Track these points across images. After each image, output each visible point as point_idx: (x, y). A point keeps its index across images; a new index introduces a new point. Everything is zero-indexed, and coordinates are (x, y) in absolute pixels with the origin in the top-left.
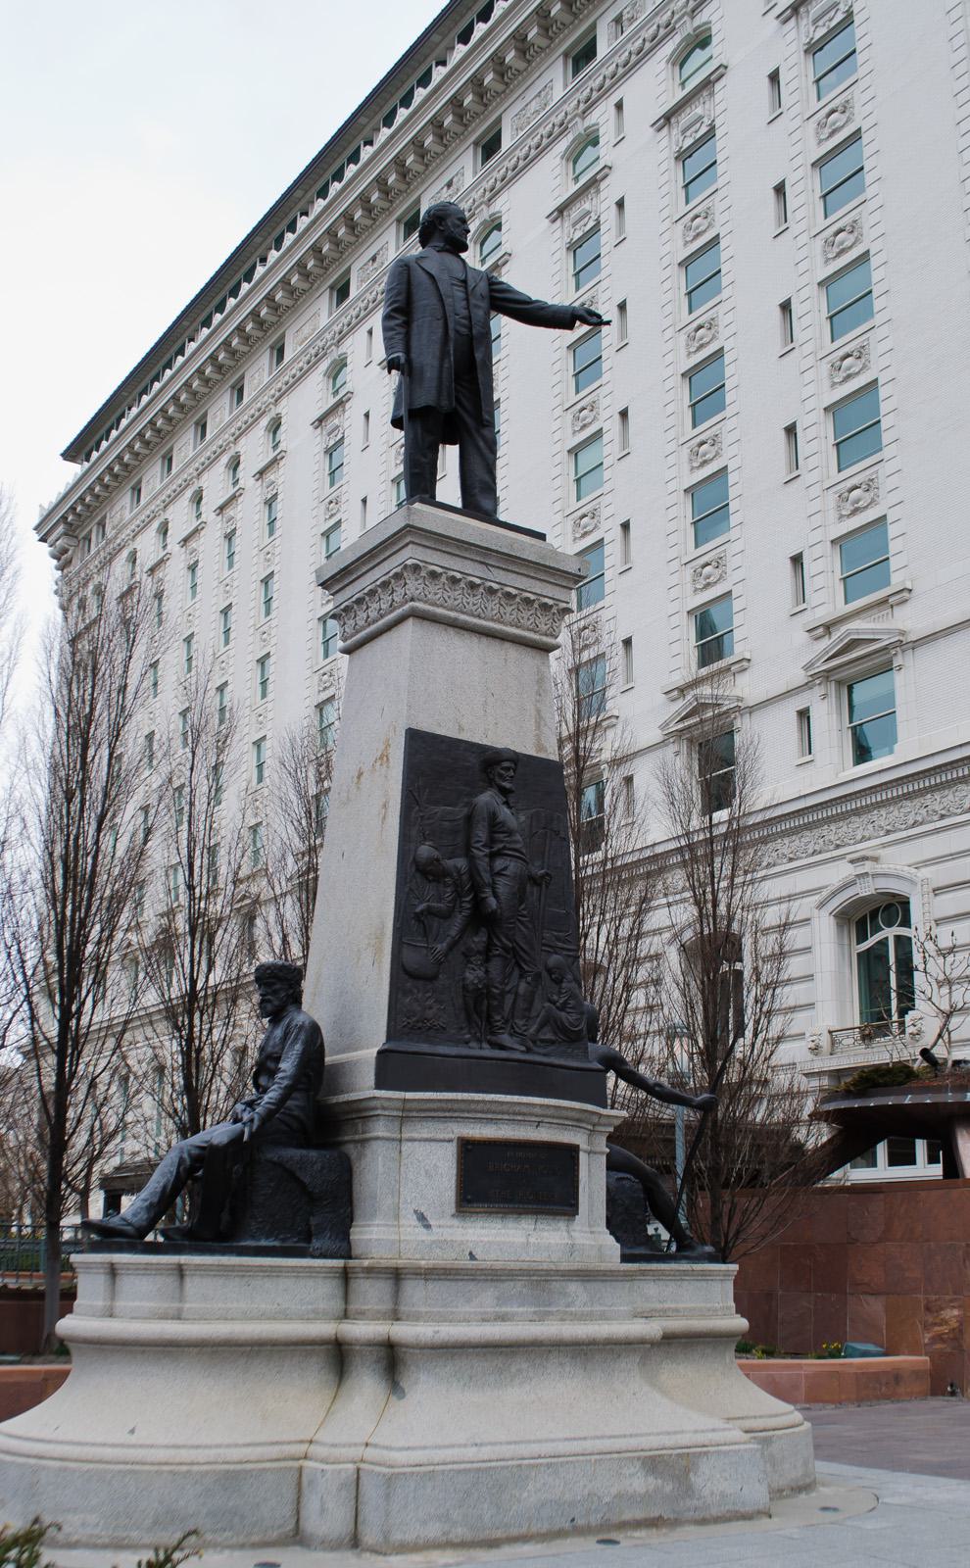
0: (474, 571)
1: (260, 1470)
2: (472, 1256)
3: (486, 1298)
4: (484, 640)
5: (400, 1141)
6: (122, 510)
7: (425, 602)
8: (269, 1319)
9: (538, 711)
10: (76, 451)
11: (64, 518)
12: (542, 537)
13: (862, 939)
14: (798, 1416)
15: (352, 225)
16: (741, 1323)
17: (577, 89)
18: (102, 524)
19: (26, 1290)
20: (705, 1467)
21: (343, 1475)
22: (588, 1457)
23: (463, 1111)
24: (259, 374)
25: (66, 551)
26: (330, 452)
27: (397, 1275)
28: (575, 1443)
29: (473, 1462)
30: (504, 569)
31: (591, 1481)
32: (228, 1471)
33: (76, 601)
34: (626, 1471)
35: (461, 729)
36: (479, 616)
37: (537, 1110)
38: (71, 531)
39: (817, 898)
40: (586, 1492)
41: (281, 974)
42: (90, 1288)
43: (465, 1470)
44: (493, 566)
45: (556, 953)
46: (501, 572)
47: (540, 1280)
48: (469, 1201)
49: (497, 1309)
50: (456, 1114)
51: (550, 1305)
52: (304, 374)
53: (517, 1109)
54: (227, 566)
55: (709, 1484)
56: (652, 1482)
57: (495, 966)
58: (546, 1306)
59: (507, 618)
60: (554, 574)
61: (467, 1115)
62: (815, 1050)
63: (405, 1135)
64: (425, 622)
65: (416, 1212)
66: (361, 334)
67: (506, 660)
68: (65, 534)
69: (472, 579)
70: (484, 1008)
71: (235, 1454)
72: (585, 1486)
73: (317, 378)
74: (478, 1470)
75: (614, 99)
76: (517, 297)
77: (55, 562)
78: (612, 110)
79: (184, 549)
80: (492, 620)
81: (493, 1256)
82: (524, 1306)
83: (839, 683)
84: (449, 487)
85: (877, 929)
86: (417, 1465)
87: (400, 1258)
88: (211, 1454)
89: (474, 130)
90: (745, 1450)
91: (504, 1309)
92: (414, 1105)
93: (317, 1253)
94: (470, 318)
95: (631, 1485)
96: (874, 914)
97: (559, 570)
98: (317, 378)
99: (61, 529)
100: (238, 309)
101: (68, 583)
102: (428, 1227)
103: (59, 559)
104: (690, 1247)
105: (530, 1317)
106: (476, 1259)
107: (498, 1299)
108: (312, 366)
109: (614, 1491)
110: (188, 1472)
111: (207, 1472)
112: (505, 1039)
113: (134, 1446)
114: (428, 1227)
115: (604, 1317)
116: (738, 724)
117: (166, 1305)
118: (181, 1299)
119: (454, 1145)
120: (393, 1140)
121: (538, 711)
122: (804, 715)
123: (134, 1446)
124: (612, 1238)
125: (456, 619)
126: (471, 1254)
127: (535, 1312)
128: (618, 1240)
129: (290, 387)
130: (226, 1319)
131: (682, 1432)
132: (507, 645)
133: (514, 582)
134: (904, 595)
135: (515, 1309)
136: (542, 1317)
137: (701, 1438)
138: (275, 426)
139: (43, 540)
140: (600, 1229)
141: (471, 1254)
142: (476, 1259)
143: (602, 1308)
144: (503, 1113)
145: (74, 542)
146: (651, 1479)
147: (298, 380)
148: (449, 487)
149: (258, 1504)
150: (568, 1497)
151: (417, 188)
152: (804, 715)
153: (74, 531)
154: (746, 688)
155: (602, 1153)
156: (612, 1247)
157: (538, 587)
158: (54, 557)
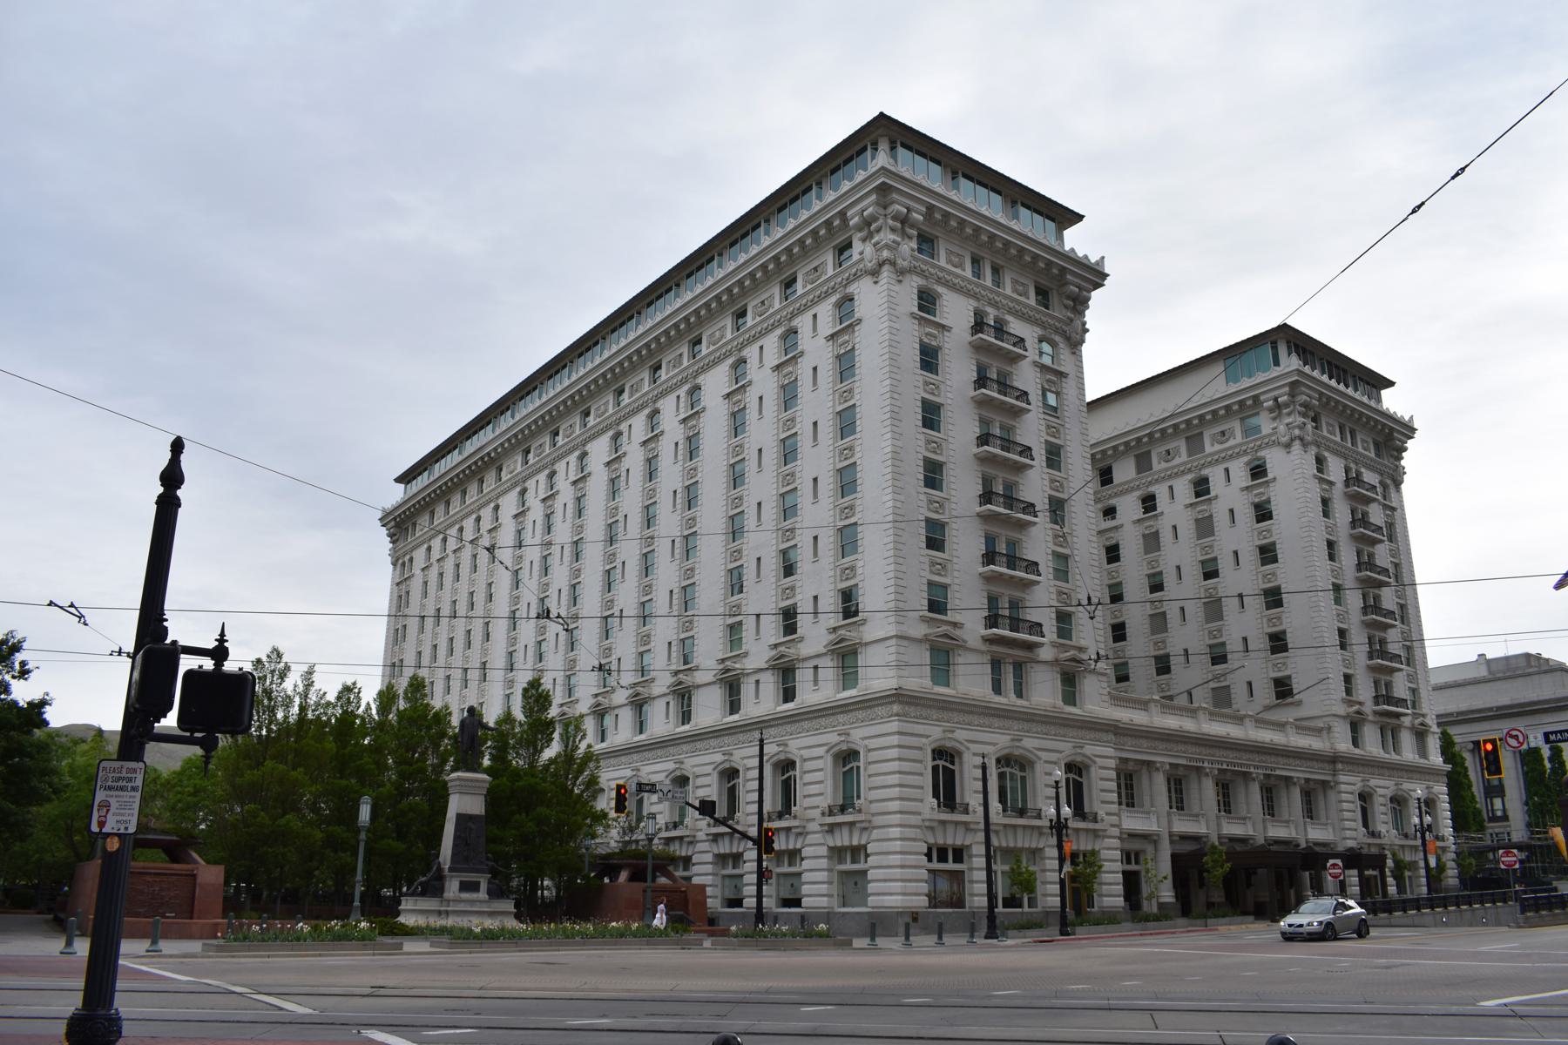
3: (462, 904)
13: (783, 775)
15: (597, 385)
17: (653, 390)
18: (414, 525)
19: (1384, 912)
26: (734, 415)
27: (449, 901)
38: (397, 526)
39: (825, 748)
42: (403, 903)
47: (472, 902)
54: (688, 458)
62: (823, 814)
66: (672, 398)
75: (759, 344)
78: (675, 399)
79: (682, 426)
83: (838, 654)
85: (788, 772)
96: (849, 755)
99: (393, 523)
101: (395, 552)
116: (859, 650)
122: (668, 703)
134: (746, 654)
152: (668, 703)
154: (805, 649)
158: (388, 536)
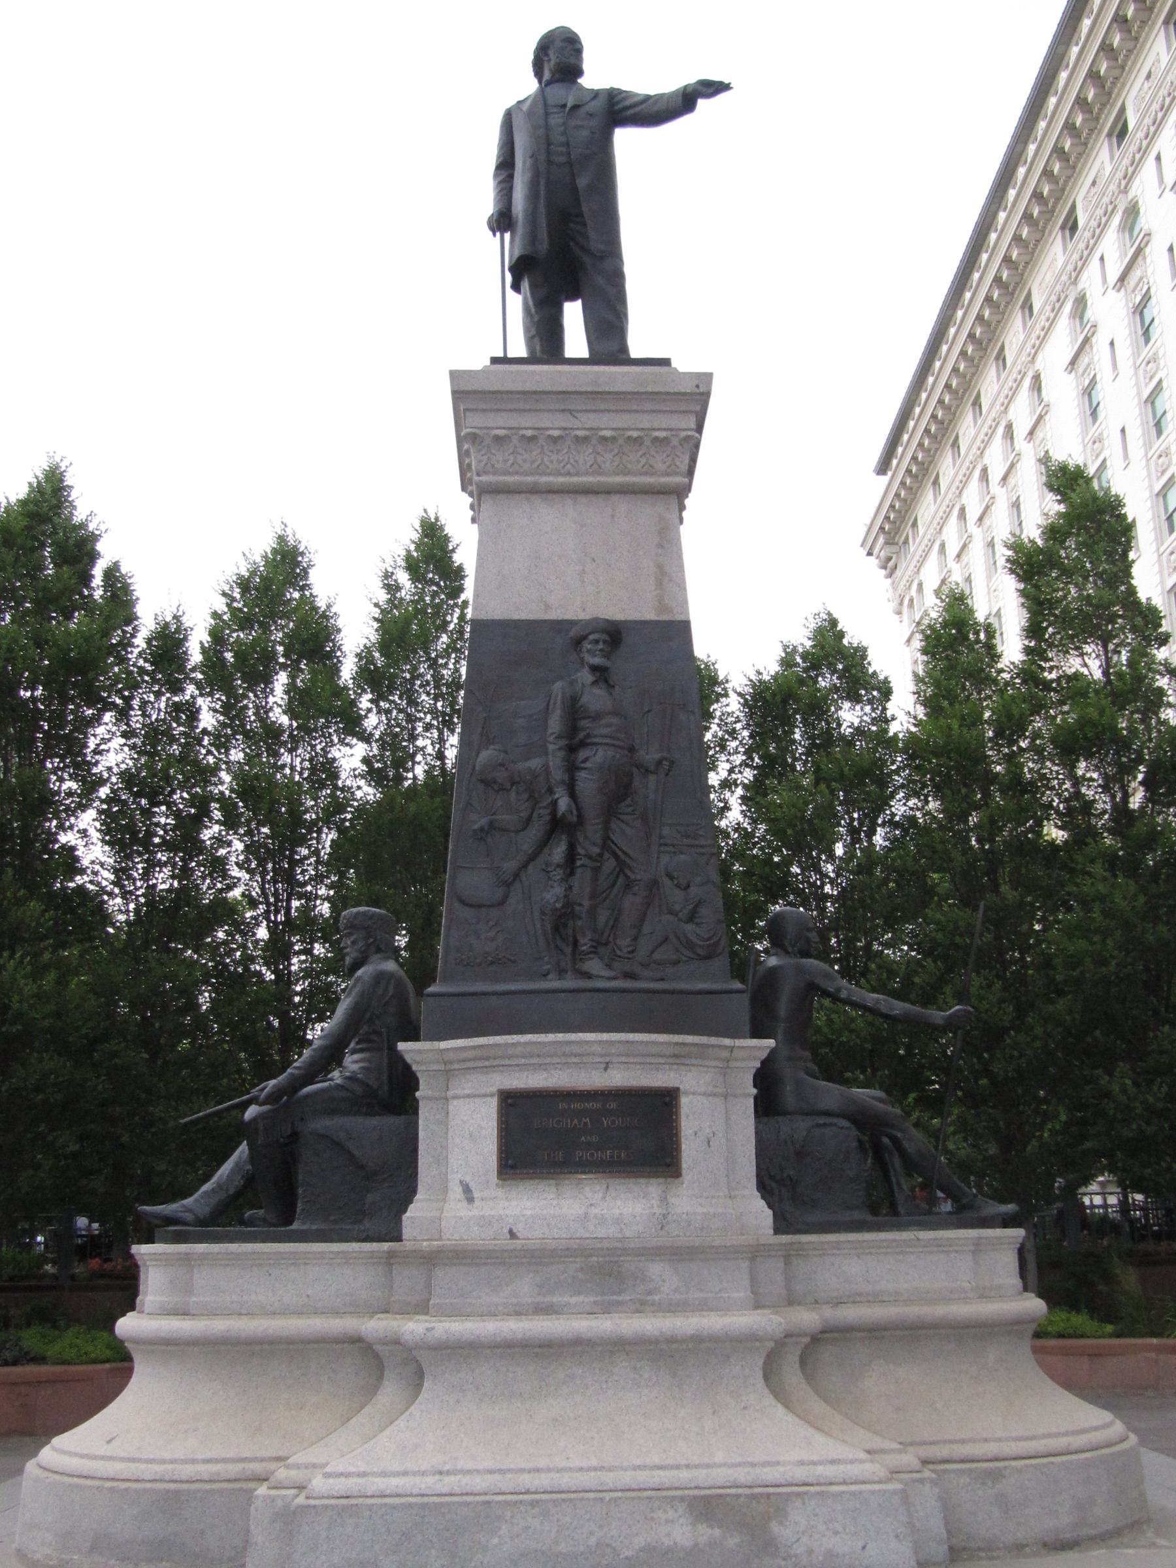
0: (553, 423)
1: (206, 1491)
2: (512, 1235)
4: (582, 499)
5: (446, 1099)
6: (927, 508)
7: (495, 473)
8: (294, 1313)
9: (660, 567)
10: (883, 467)
11: (882, 528)
12: (665, 362)
14: (1119, 1427)
16: (1035, 1305)
20: (798, 1516)
21: (279, 1502)
22: (601, 1495)
23: (503, 1058)
24: (1015, 336)
25: (889, 559)
28: (1054, 1430)
29: (423, 1495)
30: (595, 411)
31: (601, 1527)
32: (168, 1491)
33: (906, 602)
34: (660, 1515)
35: (547, 607)
36: (569, 474)
37: (597, 1049)
40: (593, 1541)
41: (356, 922)
43: (410, 1506)
44: (581, 411)
45: (682, 853)
46: (592, 416)
48: (512, 1167)
49: (540, 1299)
50: (496, 1062)
51: (620, 1293)
52: (1052, 322)
53: (567, 1049)
55: (805, 1539)
56: (706, 1533)
57: (581, 881)
58: (614, 1294)
59: (661, 466)
60: (664, 400)
61: (507, 1062)
63: (450, 1094)
64: (500, 496)
65: (461, 1182)
67: (613, 516)
68: (887, 543)
69: (524, 432)
70: (570, 932)
71: (187, 1471)
72: (592, 1533)
73: (1064, 322)
74: (424, 1506)
76: (639, 98)
77: (883, 572)
80: (587, 474)
81: (537, 1234)
82: (579, 1294)
84: (576, 342)
86: (342, 1497)
87: (440, 1239)
88: (158, 1469)
89: (1160, 10)
90: (873, 1492)
91: (548, 1299)
92: (451, 1056)
93: (363, 1236)
94: (567, 144)
95: (668, 1535)
97: (668, 393)
98: (1064, 322)
99: (881, 540)
100: (983, 282)
102: (470, 1200)
103: (885, 568)
104: (970, 1207)
105: (588, 1309)
106: (517, 1238)
107: (540, 1286)
108: (1057, 311)
109: (639, 1542)
110: (126, 1490)
111: (145, 1490)
112: (594, 965)
113: (111, 1458)
114: (470, 1200)
115: (704, 1306)
117: (176, 1299)
118: (188, 1290)
119: (494, 1102)
120: (437, 1099)
121: (660, 567)
123: (111, 1458)
124: (763, 1203)
125: (536, 484)
126: (511, 1232)
127: (595, 1302)
128: (770, 1206)
129: (1043, 340)
130: (240, 1314)
131: (778, 1463)
132: (615, 498)
133: (607, 423)
135: (566, 1299)
136: (607, 1309)
137: (800, 1474)
138: (1037, 384)
139: (870, 554)
140: (746, 1192)
141: (511, 1232)
142: (517, 1238)
143: (702, 1295)
144: (551, 1056)
145: (895, 549)
146: (702, 1528)
147: (1047, 331)
148: (576, 342)
149: (202, 1532)
150: (563, 1547)
151: (1119, 94)
153: (894, 538)
155: (749, 1095)
156: (760, 1214)
157: (645, 421)
